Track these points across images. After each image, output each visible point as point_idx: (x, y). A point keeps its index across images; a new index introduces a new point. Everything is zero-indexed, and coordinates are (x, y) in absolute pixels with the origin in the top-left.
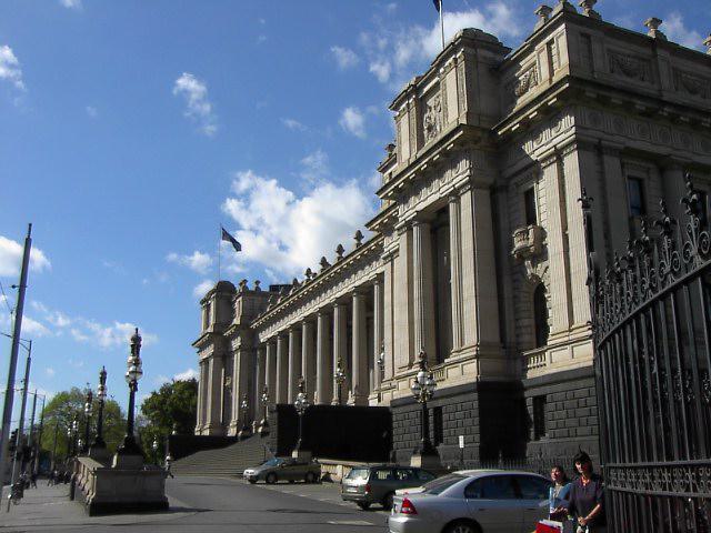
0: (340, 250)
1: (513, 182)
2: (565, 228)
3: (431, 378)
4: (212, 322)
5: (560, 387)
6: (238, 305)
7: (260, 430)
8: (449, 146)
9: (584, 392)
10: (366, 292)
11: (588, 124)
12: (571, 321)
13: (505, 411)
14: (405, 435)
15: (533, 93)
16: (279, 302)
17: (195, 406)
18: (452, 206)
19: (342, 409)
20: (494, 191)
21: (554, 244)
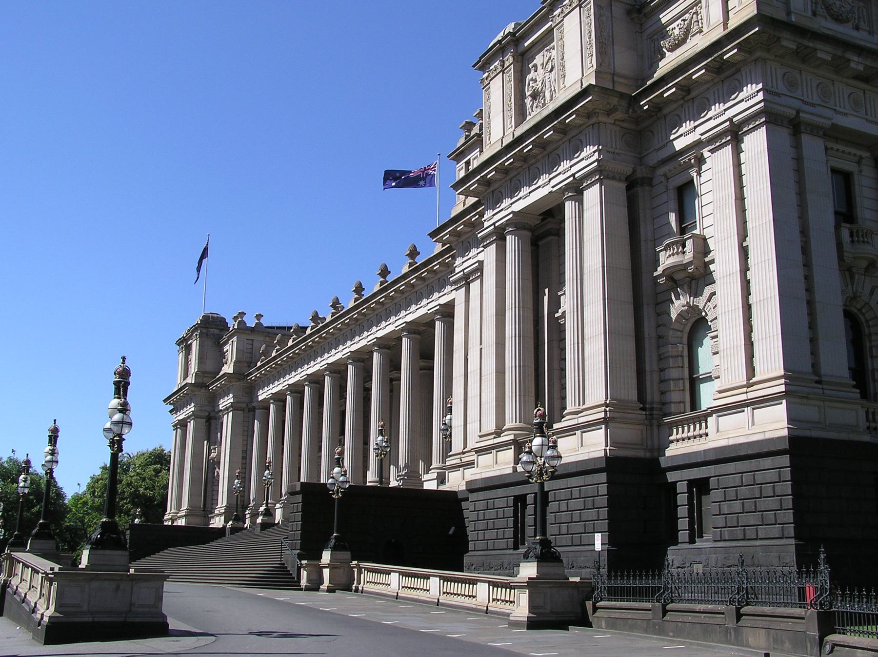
0: (336, 304)
1: (661, 171)
2: (743, 234)
3: (555, 447)
4: (193, 368)
5: (731, 467)
6: (231, 349)
7: (259, 520)
8: (570, 118)
9: (772, 475)
10: (421, 332)
11: (781, 88)
12: (751, 370)
13: (644, 504)
14: (482, 526)
15: (697, 44)
16: (290, 343)
17: (166, 487)
18: (570, 208)
19: (382, 492)
20: (632, 184)
21: (724, 263)
